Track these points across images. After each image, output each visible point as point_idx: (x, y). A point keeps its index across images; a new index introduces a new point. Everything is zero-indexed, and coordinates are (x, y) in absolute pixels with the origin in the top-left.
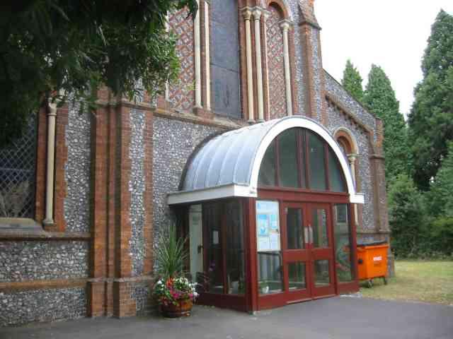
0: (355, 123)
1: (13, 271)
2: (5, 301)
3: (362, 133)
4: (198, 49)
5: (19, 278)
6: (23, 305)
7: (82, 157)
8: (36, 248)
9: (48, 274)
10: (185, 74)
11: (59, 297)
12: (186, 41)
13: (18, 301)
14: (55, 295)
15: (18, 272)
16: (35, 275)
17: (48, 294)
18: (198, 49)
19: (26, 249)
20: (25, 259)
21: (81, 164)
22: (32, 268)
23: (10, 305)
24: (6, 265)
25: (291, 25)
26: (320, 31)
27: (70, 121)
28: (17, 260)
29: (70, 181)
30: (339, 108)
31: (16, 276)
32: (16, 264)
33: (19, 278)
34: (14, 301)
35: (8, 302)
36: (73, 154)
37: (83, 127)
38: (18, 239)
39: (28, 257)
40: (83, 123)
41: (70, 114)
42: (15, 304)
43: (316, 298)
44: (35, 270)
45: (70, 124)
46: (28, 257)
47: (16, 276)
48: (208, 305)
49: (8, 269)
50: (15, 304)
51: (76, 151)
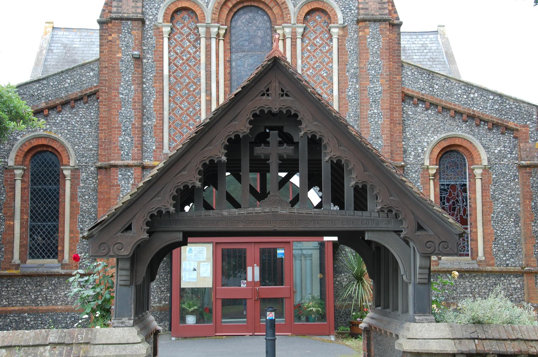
0: (486, 122)
1: (37, 298)
2: (28, 320)
3: (502, 133)
4: (203, 95)
5: (41, 303)
6: (42, 323)
7: (92, 210)
8: (54, 282)
9: (63, 301)
10: (191, 122)
11: (70, 318)
12: (192, 89)
13: (38, 320)
14: (66, 317)
15: (40, 299)
16: (53, 302)
17: (61, 316)
18: (203, 95)
19: (47, 283)
20: (45, 290)
21: (91, 215)
22: (51, 297)
23: (32, 323)
24: (31, 294)
25: (343, 28)
26: (98, 18)
27: (81, 182)
28: (40, 291)
29: (81, 229)
30: (445, 109)
31: (39, 302)
32: (39, 293)
33: (41, 303)
34: (34, 320)
35: (31, 321)
36: (84, 208)
37: (92, 185)
38: (41, 275)
39: (48, 288)
40: (93, 182)
41: (81, 178)
42: (36, 322)
43: (256, 334)
44: (53, 298)
45: (82, 185)
46: (48, 288)
47: (39, 302)
48: (508, 355)
49: (33, 297)
50: (36, 322)
51: (87, 205)
